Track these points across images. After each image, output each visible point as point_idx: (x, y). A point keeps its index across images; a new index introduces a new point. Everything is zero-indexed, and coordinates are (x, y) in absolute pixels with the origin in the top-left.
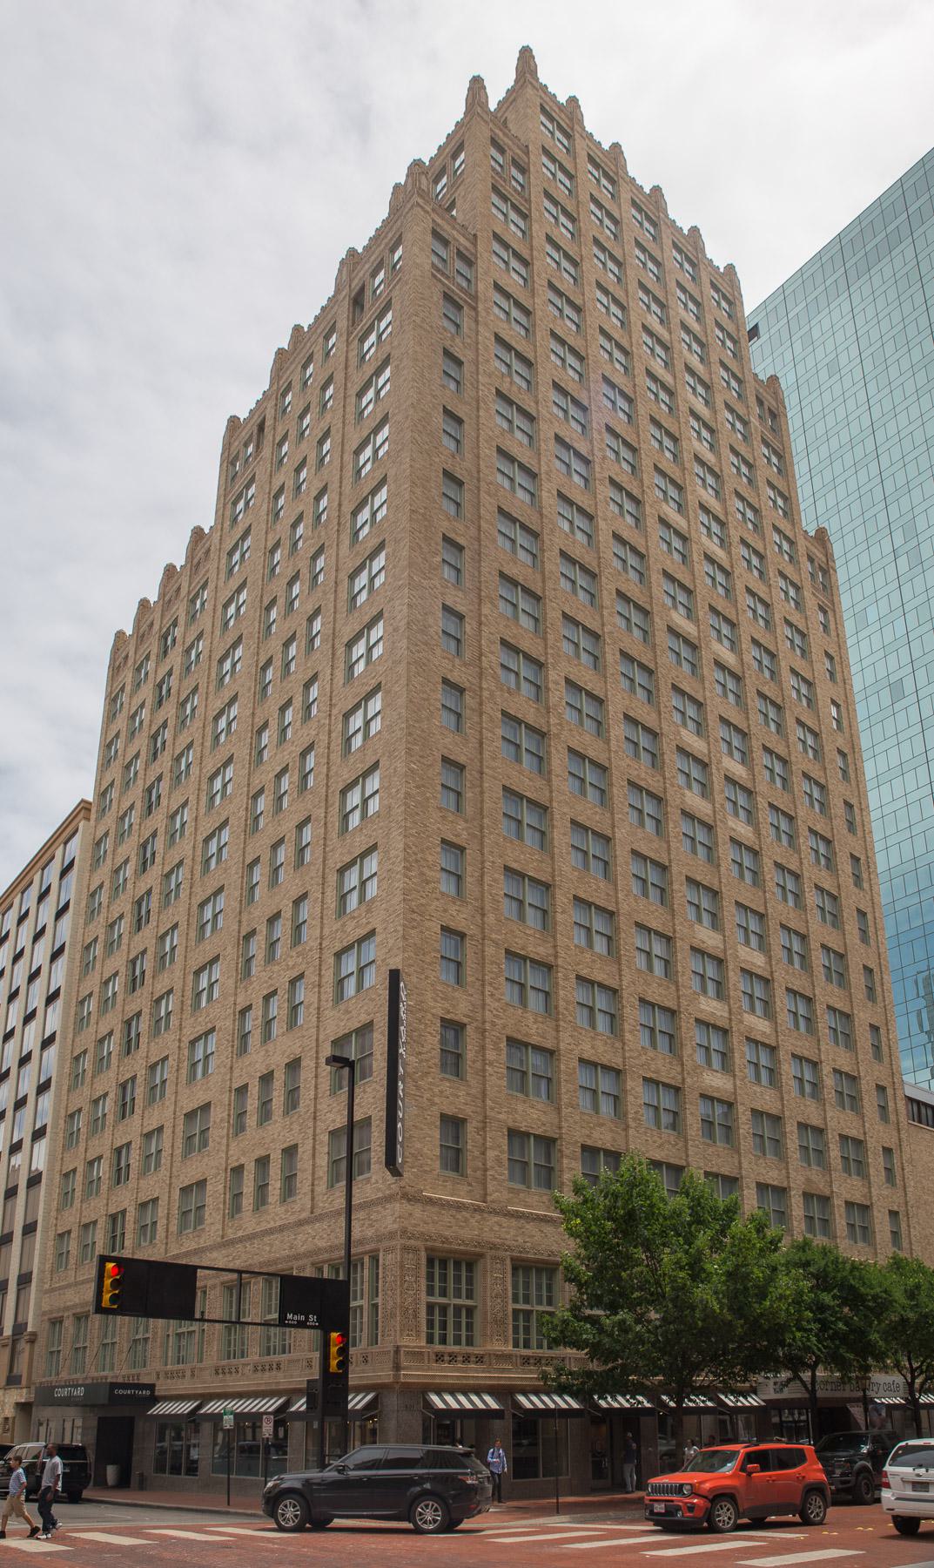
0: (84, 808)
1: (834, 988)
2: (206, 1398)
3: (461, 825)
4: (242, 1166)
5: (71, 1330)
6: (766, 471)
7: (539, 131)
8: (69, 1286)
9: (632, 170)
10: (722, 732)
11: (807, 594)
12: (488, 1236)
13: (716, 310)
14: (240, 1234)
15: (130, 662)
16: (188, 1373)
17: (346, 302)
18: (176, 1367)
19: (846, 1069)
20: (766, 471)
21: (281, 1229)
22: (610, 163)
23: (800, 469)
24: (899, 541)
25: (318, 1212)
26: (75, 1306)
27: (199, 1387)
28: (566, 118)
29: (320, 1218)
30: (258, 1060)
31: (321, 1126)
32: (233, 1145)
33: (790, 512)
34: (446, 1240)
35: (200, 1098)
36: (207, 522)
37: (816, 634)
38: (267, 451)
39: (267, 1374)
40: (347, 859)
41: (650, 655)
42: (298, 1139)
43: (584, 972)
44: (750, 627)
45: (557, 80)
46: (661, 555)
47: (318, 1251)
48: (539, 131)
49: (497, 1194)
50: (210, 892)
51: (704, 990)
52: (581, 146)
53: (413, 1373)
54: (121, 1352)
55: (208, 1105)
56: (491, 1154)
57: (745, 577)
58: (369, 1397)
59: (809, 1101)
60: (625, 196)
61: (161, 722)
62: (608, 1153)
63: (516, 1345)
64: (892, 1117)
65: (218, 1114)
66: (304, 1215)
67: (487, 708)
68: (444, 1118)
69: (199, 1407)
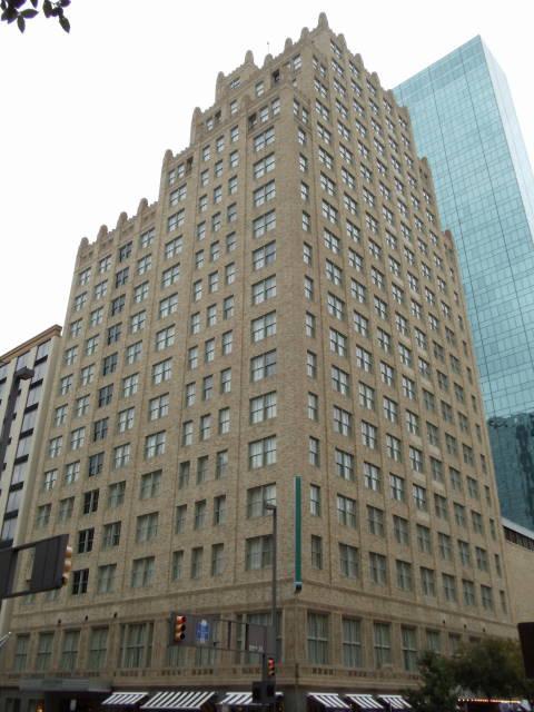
0: (57, 329)
1: (469, 466)
2: (153, 690)
3: (316, 384)
4: (182, 552)
5: (37, 642)
6: (425, 204)
7: (329, 51)
8: (37, 614)
9: (366, 66)
10: (416, 334)
11: (445, 263)
12: (332, 603)
13: (350, 73)
14: (180, 591)
15: (95, 257)
16: (140, 674)
17: (245, 119)
18: (134, 669)
19: (476, 510)
20: (425, 204)
21: (211, 591)
22: (356, 62)
23: (439, 204)
24: (462, 215)
25: (238, 584)
26: (42, 627)
27: (149, 682)
28: (339, 43)
29: (240, 587)
30: (192, 493)
31: (240, 535)
32: (175, 538)
33: (435, 222)
34: (315, 604)
35: (150, 509)
36: (153, 197)
37: (450, 283)
38: (194, 174)
39: (202, 676)
40: (257, 395)
41: (340, 261)
42: (224, 540)
43: (367, 459)
44: (425, 282)
45: (336, 27)
46: (389, 249)
47: (240, 606)
48: (329, 51)
49: (336, 580)
50: (157, 395)
51: (415, 468)
52: (346, 56)
53: (305, 680)
54: (82, 658)
55: (156, 513)
56: (333, 557)
57: (421, 257)
58: (212, 694)
59: (462, 528)
60: (364, 78)
61: (119, 294)
62: (352, 548)
63: (346, 665)
64: (498, 538)
65: (163, 519)
66: (229, 584)
67: (324, 326)
68: (313, 537)
69: (146, 699)
